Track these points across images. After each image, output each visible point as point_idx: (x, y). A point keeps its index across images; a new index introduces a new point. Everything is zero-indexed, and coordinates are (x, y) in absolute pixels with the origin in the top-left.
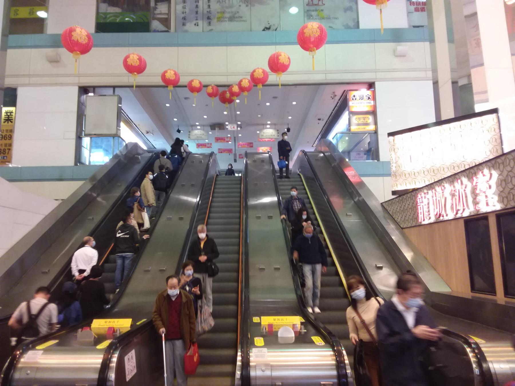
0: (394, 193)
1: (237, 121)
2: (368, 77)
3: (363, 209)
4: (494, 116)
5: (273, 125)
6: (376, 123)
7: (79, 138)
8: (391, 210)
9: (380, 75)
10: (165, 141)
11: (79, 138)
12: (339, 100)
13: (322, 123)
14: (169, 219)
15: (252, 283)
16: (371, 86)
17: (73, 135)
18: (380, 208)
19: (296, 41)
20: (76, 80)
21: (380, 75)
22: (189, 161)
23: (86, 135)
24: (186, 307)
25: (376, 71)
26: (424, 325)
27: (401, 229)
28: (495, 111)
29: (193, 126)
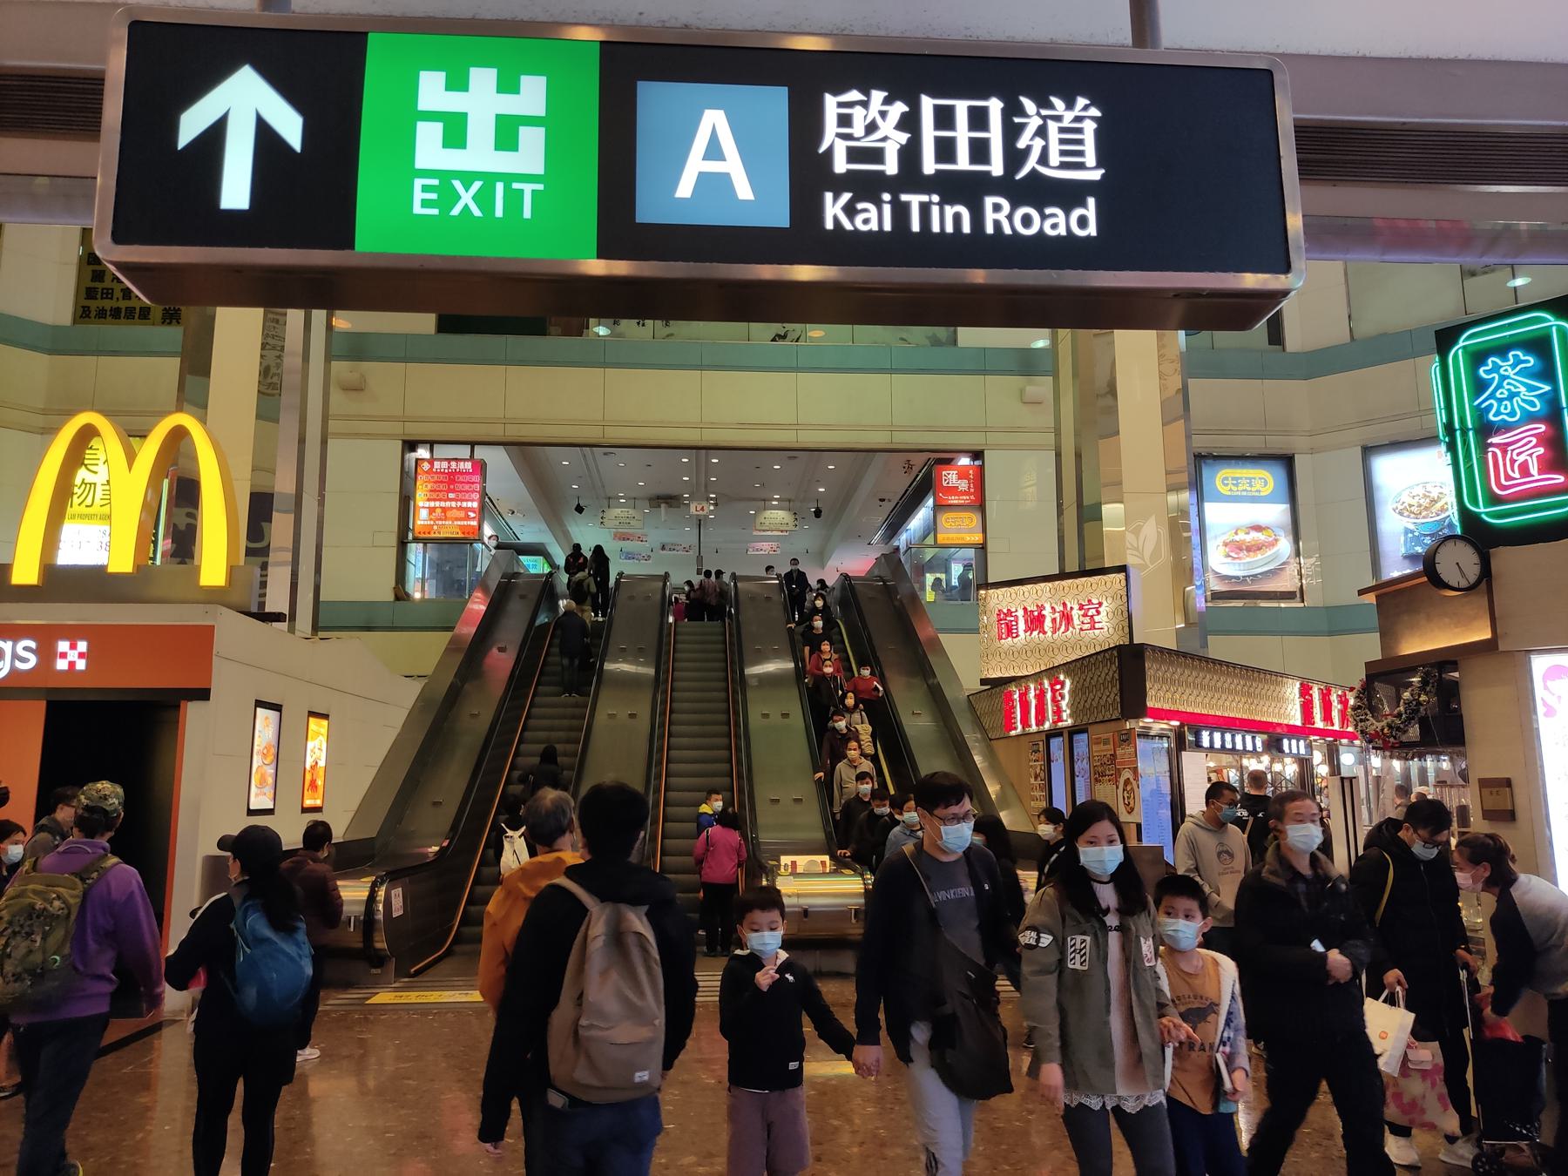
0: (984, 682)
1: (708, 492)
2: (974, 441)
3: (938, 700)
4: (1122, 576)
5: (788, 504)
6: (984, 531)
7: (402, 545)
8: (981, 707)
9: (992, 438)
10: (544, 526)
11: (402, 545)
13: (888, 506)
14: (612, 716)
15: (761, 820)
16: (977, 455)
17: (393, 540)
18: (965, 705)
19: (819, 835)
20: (397, 428)
21: (992, 438)
22: (622, 597)
23: (416, 540)
24: (1438, 505)
25: (986, 430)
27: (988, 741)
28: (1123, 569)
29: (610, 500)
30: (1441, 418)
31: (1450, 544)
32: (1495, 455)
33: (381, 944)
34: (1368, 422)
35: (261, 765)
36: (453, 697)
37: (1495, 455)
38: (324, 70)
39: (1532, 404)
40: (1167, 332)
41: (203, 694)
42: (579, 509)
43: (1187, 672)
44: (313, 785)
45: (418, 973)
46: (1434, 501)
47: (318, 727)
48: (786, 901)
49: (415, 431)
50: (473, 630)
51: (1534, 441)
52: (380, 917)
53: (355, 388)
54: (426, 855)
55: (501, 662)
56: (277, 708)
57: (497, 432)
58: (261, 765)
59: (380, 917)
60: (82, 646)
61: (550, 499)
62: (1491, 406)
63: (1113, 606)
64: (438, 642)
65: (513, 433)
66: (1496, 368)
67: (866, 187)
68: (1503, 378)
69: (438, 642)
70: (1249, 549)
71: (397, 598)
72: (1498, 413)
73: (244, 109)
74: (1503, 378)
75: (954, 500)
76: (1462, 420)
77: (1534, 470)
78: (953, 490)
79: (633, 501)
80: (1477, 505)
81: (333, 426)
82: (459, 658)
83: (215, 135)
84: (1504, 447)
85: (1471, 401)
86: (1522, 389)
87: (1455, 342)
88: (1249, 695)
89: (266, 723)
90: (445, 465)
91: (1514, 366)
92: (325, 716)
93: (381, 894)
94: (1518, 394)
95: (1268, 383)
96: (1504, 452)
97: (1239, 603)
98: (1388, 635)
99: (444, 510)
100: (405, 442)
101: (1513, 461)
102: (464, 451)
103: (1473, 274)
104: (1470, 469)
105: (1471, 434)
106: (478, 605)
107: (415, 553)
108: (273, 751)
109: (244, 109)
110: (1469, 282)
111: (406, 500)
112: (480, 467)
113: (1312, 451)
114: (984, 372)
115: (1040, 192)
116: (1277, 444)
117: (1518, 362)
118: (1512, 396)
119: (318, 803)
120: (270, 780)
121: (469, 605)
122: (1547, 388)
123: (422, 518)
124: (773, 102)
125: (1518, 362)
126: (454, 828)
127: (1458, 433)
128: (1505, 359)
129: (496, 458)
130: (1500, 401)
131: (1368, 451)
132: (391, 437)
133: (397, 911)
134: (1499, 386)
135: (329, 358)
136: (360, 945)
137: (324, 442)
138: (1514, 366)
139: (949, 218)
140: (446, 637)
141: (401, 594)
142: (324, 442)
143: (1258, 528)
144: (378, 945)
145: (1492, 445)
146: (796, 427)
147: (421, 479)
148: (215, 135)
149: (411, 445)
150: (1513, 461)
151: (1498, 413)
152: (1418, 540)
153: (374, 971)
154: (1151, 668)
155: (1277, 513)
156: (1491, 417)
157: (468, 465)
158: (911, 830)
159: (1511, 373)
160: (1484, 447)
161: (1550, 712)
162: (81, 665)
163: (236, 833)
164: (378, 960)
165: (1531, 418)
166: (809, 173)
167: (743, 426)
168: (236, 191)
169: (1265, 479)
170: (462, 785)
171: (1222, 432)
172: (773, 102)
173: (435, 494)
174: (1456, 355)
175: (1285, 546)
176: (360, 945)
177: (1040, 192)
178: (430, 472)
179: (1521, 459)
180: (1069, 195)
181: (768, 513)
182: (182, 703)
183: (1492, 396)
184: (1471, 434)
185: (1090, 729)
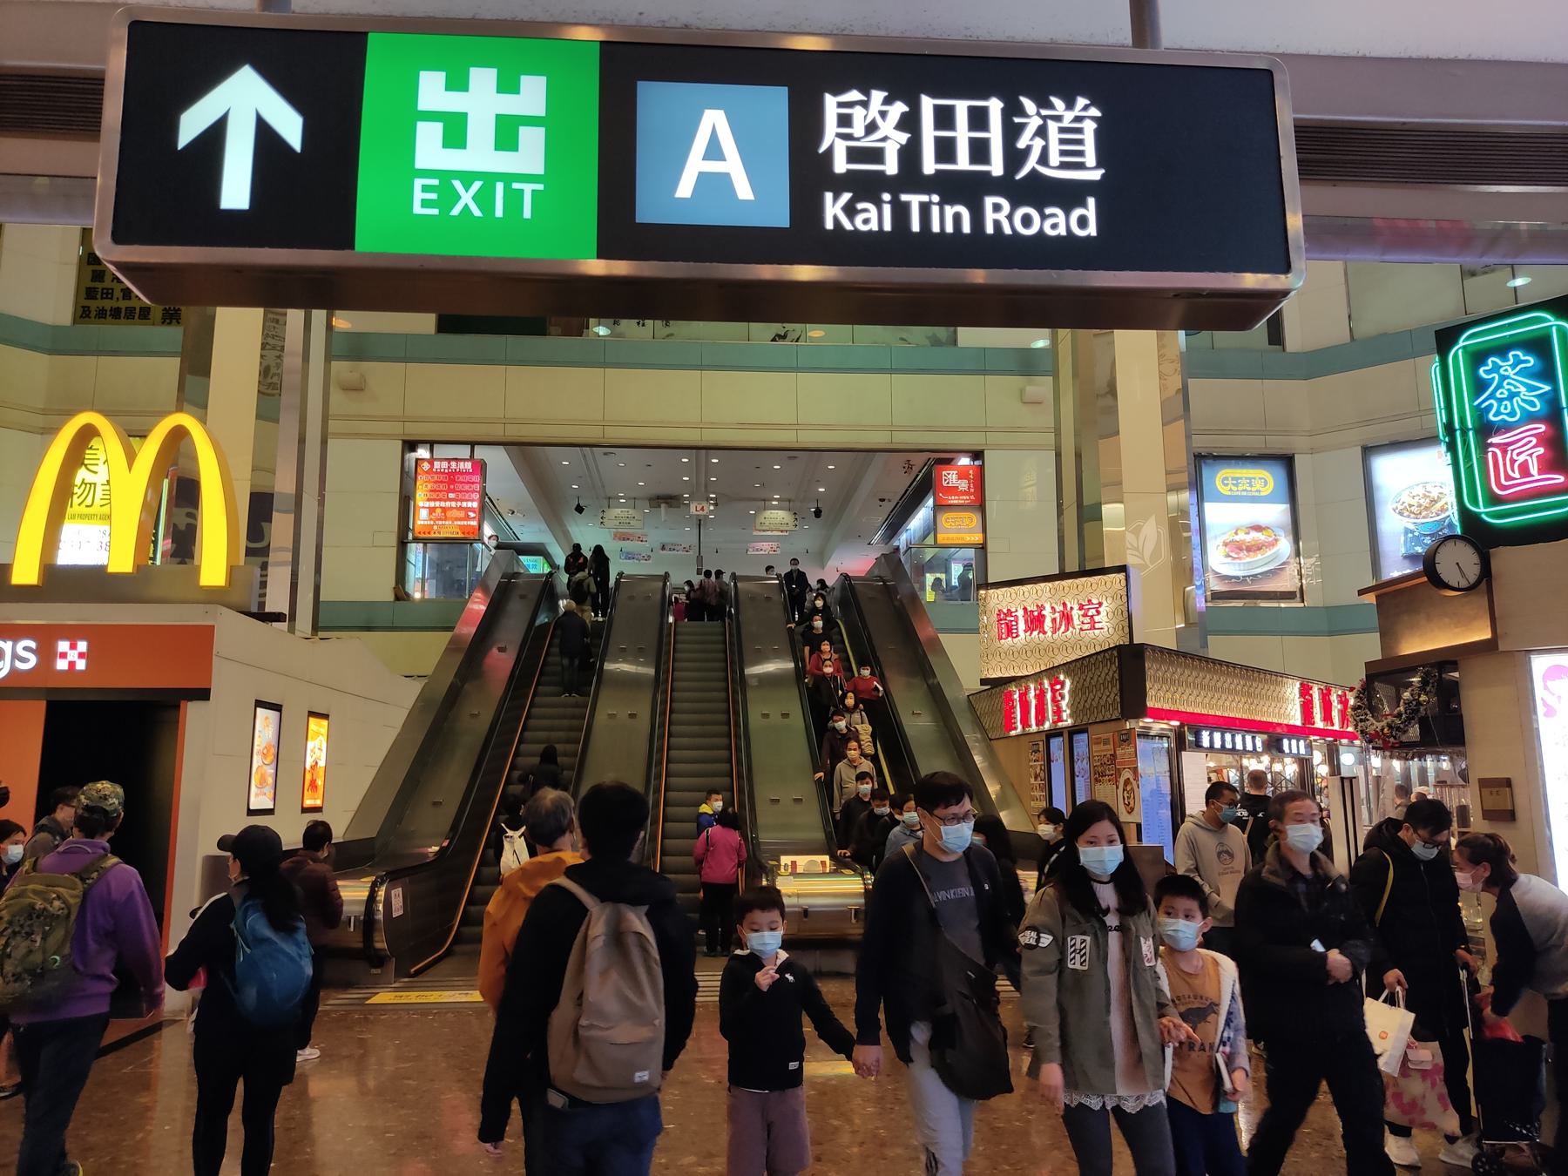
0: (984, 682)
1: (708, 492)
2: (974, 441)
3: (938, 700)
4: (1122, 576)
5: (788, 504)
6: (984, 531)
7: (402, 545)
8: (981, 707)
9: (992, 438)
11: (402, 545)
12: (798, 896)
13: (888, 506)
14: (612, 716)
15: (761, 820)
16: (977, 455)
17: (393, 540)
18: (965, 705)
19: (819, 835)
20: (397, 428)
21: (992, 438)
22: (622, 597)
23: (416, 540)
25: (986, 430)
26: (1238, 966)
27: (988, 741)
28: (1123, 569)
29: (610, 500)
30: (1441, 418)
31: (1450, 544)
32: (1495, 455)
33: (381, 944)
34: (1368, 422)
35: (261, 765)
36: (453, 697)
37: (1495, 455)
38: (324, 70)
39: (1532, 404)
40: (1167, 332)
41: (203, 694)
42: (579, 509)
43: (1187, 672)
44: (313, 785)
45: (418, 973)
46: (1434, 501)
47: (318, 727)
48: (786, 901)
49: (415, 431)
50: (473, 630)
51: (1534, 441)
52: (380, 917)
53: (355, 388)
54: (426, 855)
55: (501, 662)
56: (277, 708)
57: (497, 432)
58: (261, 765)
59: (380, 917)
60: (82, 646)
61: (550, 499)
62: (1491, 406)
63: (1113, 606)
64: (438, 642)
65: (513, 433)
66: (1496, 368)
67: (866, 187)
68: (1503, 378)
69: (438, 642)
70: (1249, 549)
71: (397, 598)
72: (1498, 413)
73: (244, 109)
74: (1503, 378)
75: (954, 500)
76: (1462, 420)
77: (1534, 470)
78: (953, 490)
79: (633, 501)
80: (1477, 505)
81: (333, 426)
82: (459, 658)
83: (215, 135)
84: (1504, 447)
85: (1471, 401)
86: (1522, 389)
87: (1455, 342)
88: (1249, 695)
89: (266, 723)
90: (445, 465)
91: (1514, 366)
92: (325, 716)
93: (381, 894)
94: (1518, 394)
95: (1268, 383)
96: (1504, 452)
97: (1239, 603)
98: (1388, 635)
99: (444, 510)
100: (405, 442)
101: (1513, 461)
102: (464, 451)
103: (1473, 274)
104: (1470, 469)
105: (1471, 434)
106: (478, 605)
107: (415, 553)
108: (273, 751)
109: (244, 109)
110: (1469, 282)
111: (406, 500)
112: (480, 467)
113: (1312, 451)
114: (984, 372)
115: (1040, 192)
116: (1277, 444)
117: (1518, 362)
118: (1512, 396)
119: (318, 803)
120: (270, 780)
121: (469, 605)
122: (1547, 388)
123: (422, 518)
124: (773, 102)
125: (1518, 362)
126: (454, 828)
127: (1458, 433)
128: (1505, 359)
129: (496, 458)
130: (1500, 401)
131: (1368, 451)
132: (391, 437)
133: (397, 911)
134: (1499, 386)
135: (329, 358)
136: (360, 945)
137: (324, 442)
138: (1514, 366)
139: (949, 218)
140: (446, 637)
141: (401, 594)
142: (324, 442)
143: (1258, 528)
144: (378, 945)
145: (1492, 445)
146: (796, 427)
147: (421, 479)
148: (215, 135)
149: (411, 445)
150: (1513, 461)
151: (1498, 413)
152: (1418, 540)
153: (374, 971)
154: (1151, 668)
155: (1277, 513)
156: (1491, 417)
157: (468, 465)
158: (911, 830)
159: (1511, 373)
160: (1484, 447)
161: (1550, 712)
162: (81, 665)
163: (236, 833)
164: (378, 960)
165: (1531, 418)
166: (809, 173)
167: (743, 426)
168: (236, 191)
169: (1265, 479)
170: (462, 785)
171: (1222, 432)
172: (773, 102)
173: (435, 494)
174: (1456, 355)
175: (1285, 546)
176: (360, 945)
177: (1040, 192)
178: (430, 472)
179: (1521, 459)
180: (1069, 195)
181: (768, 513)
182: (182, 703)
183: (1492, 396)
184: (1471, 434)
185: (1090, 729)
